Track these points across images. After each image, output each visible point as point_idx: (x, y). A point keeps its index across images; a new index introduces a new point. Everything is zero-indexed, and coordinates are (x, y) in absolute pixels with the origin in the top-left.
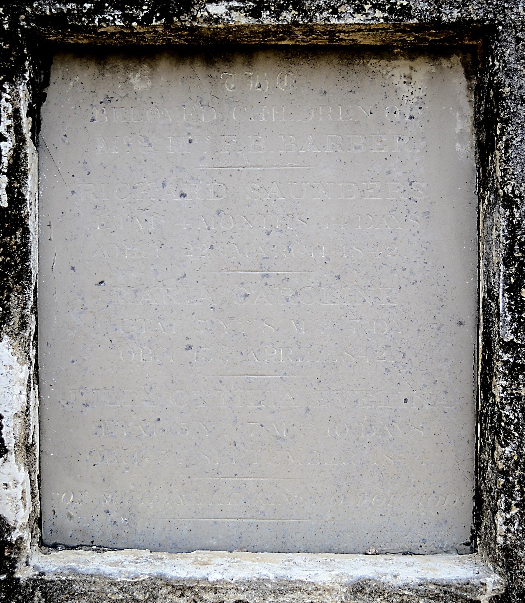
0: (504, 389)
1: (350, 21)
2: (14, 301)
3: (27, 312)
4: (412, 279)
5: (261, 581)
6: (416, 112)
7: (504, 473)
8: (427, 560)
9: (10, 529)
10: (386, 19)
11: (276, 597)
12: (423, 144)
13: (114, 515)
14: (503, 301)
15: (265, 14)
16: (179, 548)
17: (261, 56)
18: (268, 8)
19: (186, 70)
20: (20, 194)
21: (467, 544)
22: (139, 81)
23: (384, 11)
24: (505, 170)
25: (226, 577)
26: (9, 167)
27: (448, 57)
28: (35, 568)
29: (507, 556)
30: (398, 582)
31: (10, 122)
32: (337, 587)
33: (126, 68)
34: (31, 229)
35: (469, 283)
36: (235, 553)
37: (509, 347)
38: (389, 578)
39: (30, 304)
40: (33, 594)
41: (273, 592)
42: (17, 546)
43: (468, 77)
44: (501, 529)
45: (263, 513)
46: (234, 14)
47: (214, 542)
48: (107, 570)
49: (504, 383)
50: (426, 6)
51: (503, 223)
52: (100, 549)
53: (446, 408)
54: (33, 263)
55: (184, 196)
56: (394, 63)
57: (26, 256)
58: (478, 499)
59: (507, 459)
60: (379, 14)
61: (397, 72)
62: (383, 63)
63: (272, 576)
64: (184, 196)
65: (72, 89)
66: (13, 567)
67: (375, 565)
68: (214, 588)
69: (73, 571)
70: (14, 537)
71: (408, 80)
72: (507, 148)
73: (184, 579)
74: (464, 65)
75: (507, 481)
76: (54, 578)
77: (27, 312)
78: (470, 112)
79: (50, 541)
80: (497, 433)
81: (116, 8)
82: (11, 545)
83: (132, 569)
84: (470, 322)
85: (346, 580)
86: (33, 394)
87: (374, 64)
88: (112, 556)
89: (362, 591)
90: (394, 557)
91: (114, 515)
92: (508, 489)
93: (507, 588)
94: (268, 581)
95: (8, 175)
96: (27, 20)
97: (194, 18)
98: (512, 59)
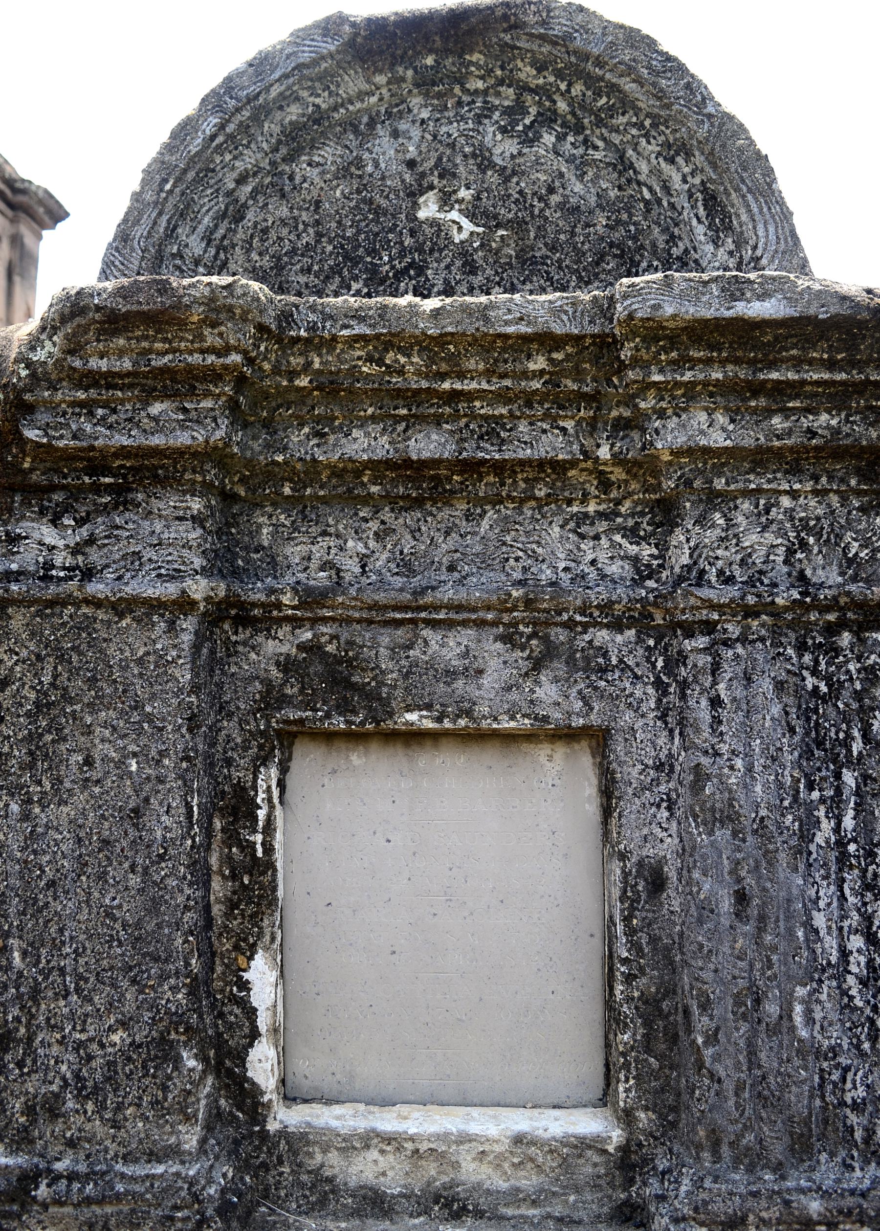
0: (622, 992)
1: (507, 726)
2: (266, 922)
3: (275, 929)
4: (556, 903)
5: (447, 1134)
6: (557, 782)
7: (624, 1054)
8: (570, 1114)
9: (262, 1093)
10: (531, 725)
11: (458, 1146)
12: (562, 804)
13: (338, 1076)
14: (620, 928)
15: (446, 721)
16: (387, 1103)
17: (444, 740)
18: (448, 717)
19: (390, 750)
20: (271, 845)
21: (600, 1100)
22: (356, 758)
23: (530, 719)
24: (619, 833)
25: (420, 1130)
26: (263, 828)
27: (579, 742)
28: (281, 1122)
29: (627, 1116)
30: (547, 1135)
31: (264, 796)
32: (503, 1138)
33: (347, 749)
34: (279, 868)
35: (596, 906)
36: (429, 1107)
37: (624, 962)
38: (541, 1131)
39: (278, 923)
40: (279, 1142)
41: (456, 1142)
42: (268, 1106)
43: (594, 757)
44: (622, 1095)
45: (449, 1076)
46: (424, 721)
47: (412, 1098)
48: (334, 1123)
49: (621, 988)
50: (560, 716)
51: (618, 872)
52: (329, 1102)
53: (582, 998)
54: (280, 893)
55: (389, 841)
56: (540, 746)
57: (274, 889)
58: (607, 1065)
59: (625, 1044)
60: (527, 721)
61: (542, 753)
62: (532, 746)
63: (454, 1130)
64: (389, 841)
65: (307, 761)
66: (265, 1121)
67: (531, 1119)
68: (412, 1139)
69: (309, 1124)
70: (266, 1098)
71: (550, 758)
72: (620, 817)
73: (390, 1132)
74: (590, 747)
75: (626, 1059)
76: (295, 1130)
77: (275, 929)
78: (595, 781)
79: (290, 1095)
80: (618, 1024)
81: (340, 714)
82: (263, 1104)
83: (352, 1123)
84: (598, 935)
85: (509, 1133)
86: (280, 987)
87: (525, 747)
88: (338, 1110)
89: (521, 1142)
90: (546, 1111)
91: (338, 1076)
92: (626, 1066)
93: (628, 1140)
94: (452, 1134)
95: (263, 833)
96: (277, 722)
97: (396, 723)
98: (622, 754)
